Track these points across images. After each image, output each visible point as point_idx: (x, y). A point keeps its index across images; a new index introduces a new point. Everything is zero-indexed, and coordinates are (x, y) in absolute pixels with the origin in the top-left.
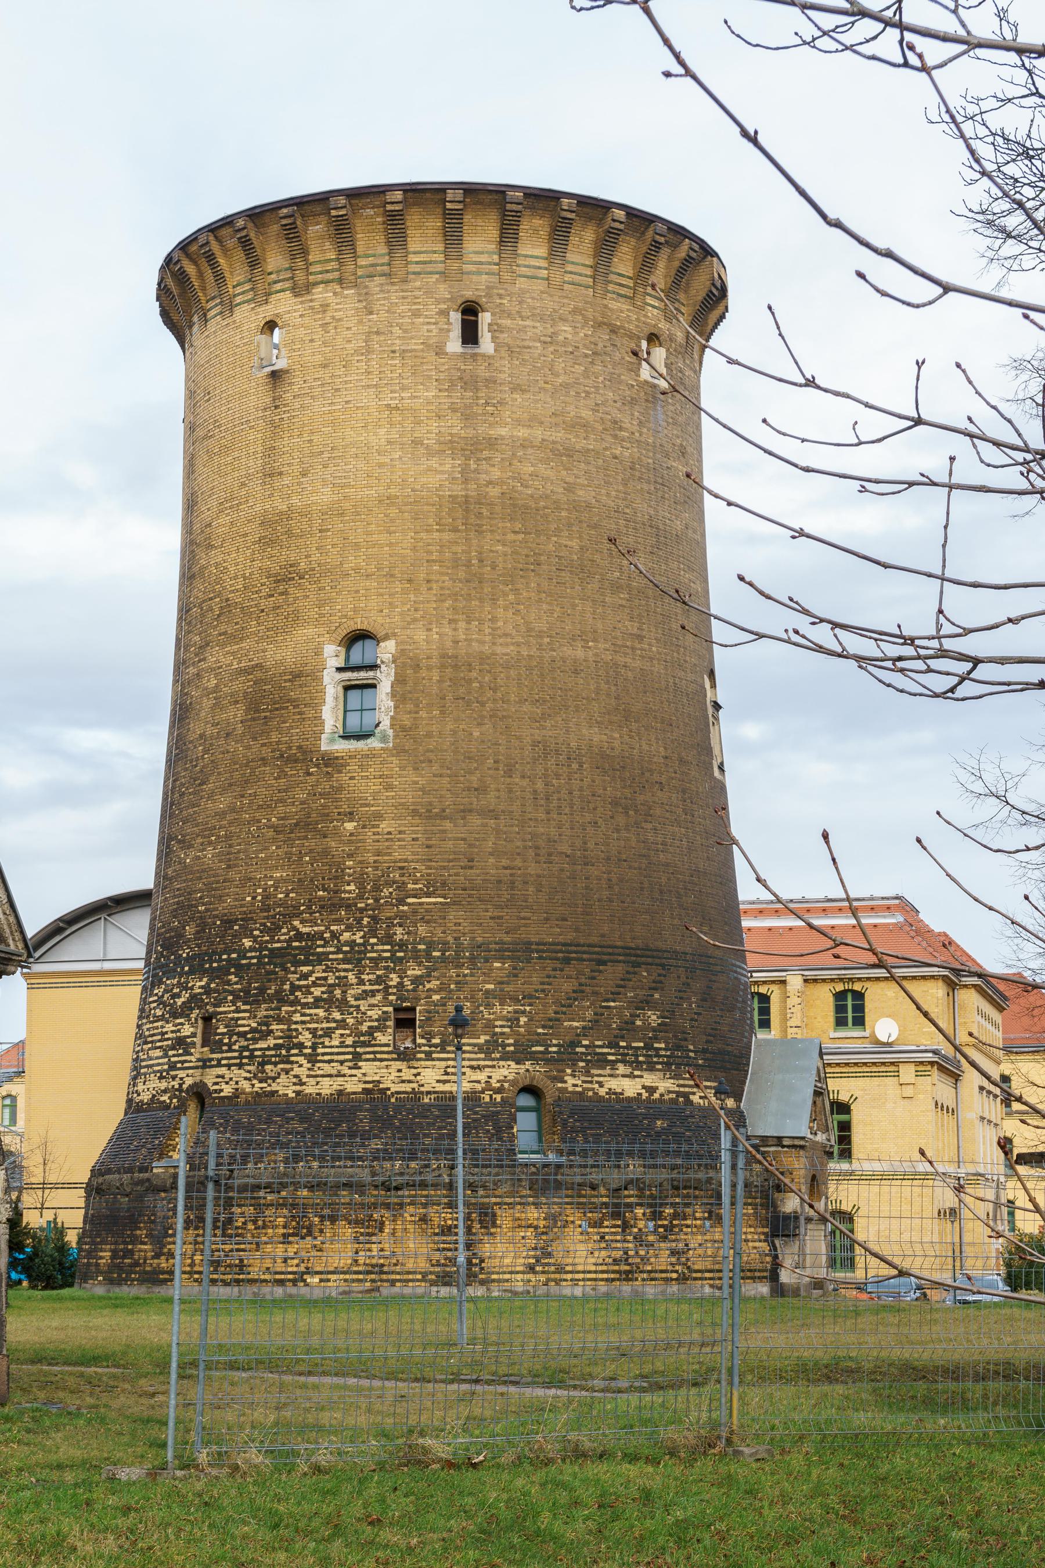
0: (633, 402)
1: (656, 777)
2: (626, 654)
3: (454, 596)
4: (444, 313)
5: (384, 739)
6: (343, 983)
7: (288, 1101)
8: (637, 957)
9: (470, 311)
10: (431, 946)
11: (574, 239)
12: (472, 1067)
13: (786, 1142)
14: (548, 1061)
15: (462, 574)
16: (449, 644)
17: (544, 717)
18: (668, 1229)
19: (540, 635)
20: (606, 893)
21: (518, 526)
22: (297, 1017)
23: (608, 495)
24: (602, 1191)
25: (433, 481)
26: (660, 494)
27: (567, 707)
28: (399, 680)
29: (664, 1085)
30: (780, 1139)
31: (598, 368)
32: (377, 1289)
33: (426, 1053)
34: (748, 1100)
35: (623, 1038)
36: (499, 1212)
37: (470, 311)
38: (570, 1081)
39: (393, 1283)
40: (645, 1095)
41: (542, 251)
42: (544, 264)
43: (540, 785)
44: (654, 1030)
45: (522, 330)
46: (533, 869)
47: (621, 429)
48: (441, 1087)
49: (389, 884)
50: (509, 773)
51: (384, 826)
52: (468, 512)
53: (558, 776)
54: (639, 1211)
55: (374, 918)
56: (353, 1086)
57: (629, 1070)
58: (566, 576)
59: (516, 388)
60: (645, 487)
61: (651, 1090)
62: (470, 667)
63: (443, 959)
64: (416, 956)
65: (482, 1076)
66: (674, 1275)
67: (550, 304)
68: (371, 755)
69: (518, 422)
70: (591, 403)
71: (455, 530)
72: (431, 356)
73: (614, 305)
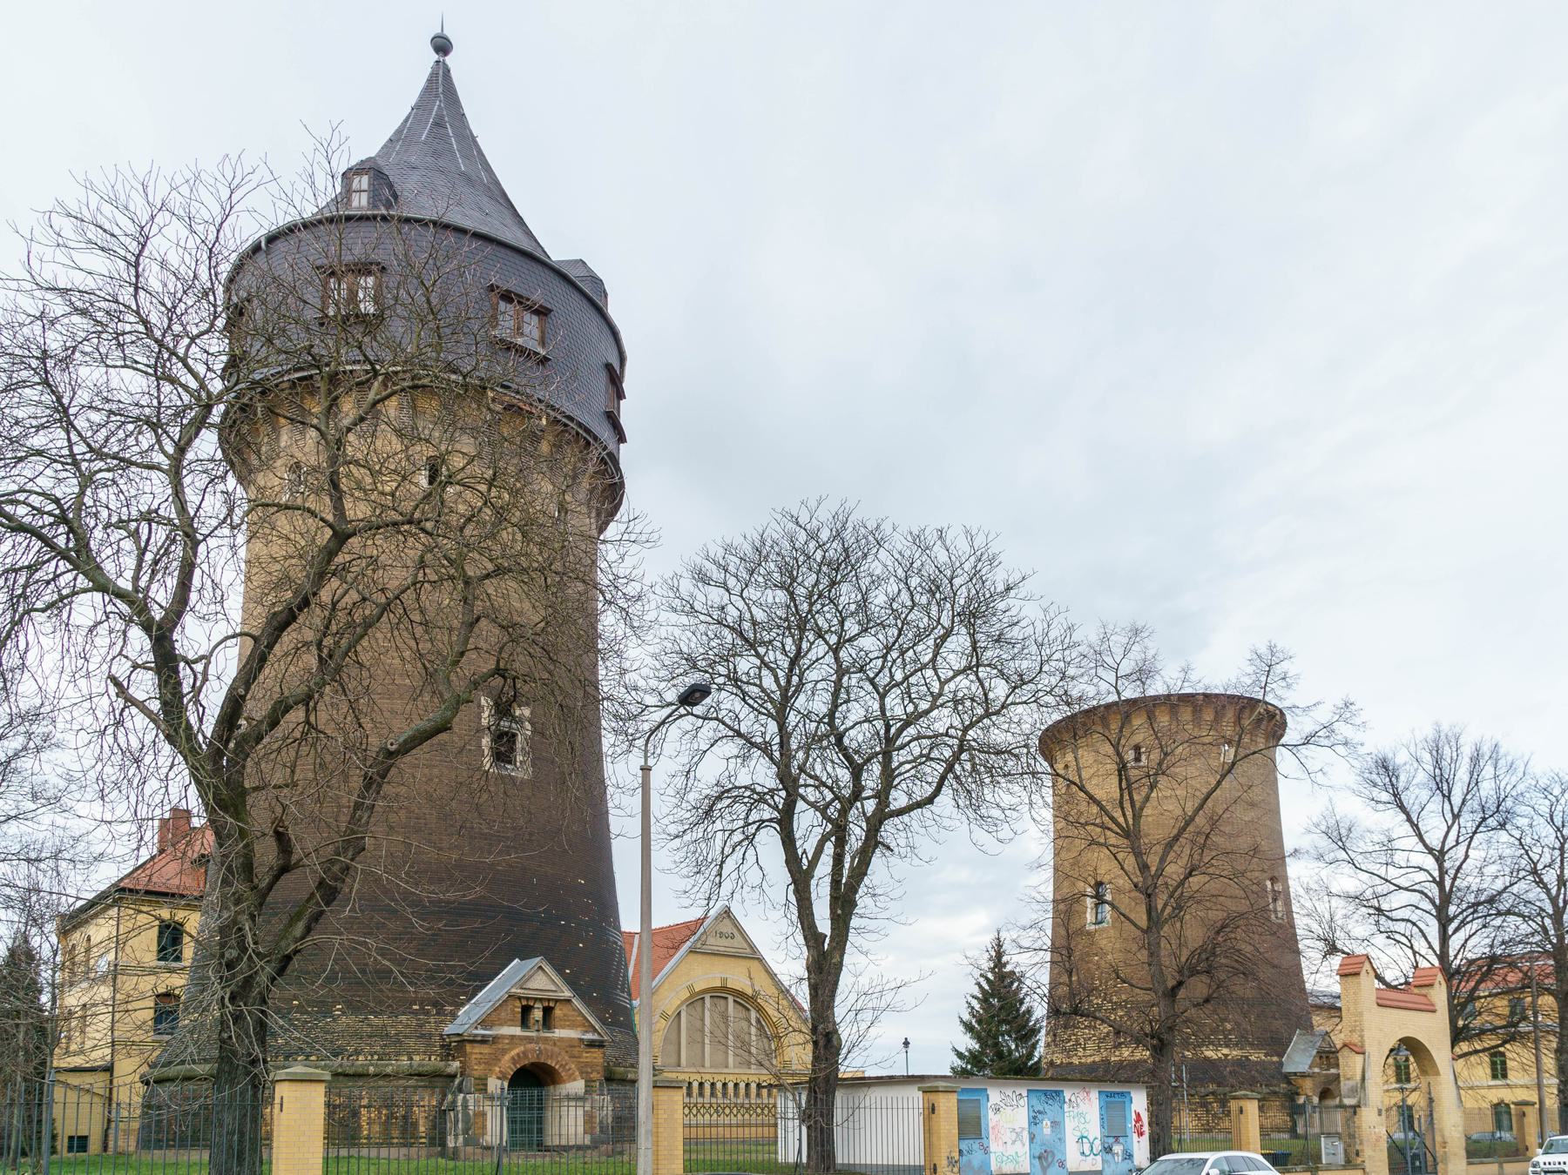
29: (1236, 1053)
68: (1104, 930)
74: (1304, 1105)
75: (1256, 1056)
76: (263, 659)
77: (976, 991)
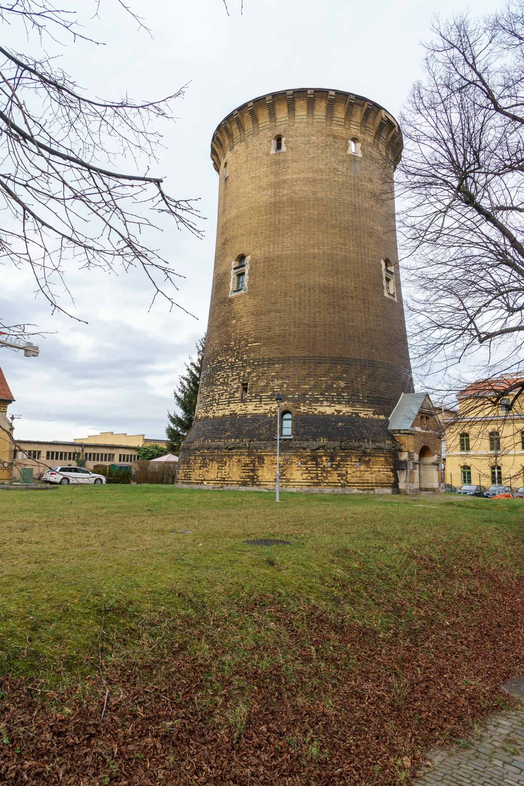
0: (344, 161)
1: (350, 294)
2: (337, 251)
3: (270, 237)
4: (270, 141)
5: (245, 290)
6: (228, 377)
7: (211, 419)
8: (334, 361)
9: (279, 139)
10: (254, 360)
11: (317, 107)
12: (265, 404)
13: (402, 432)
14: (293, 401)
15: (272, 229)
16: (267, 253)
17: (300, 275)
18: (338, 466)
19: (300, 246)
20: (323, 338)
21: (293, 208)
22: (216, 390)
23: (331, 194)
24: (308, 450)
25: (264, 199)
26: (357, 194)
27: (310, 271)
28: (251, 269)
29: (345, 410)
30: (399, 430)
31: (328, 150)
32: (222, 487)
33: (251, 400)
34: (393, 416)
35: (327, 392)
36: (266, 458)
37: (279, 139)
38: (302, 408)
39: (227, 484)
40: (336, 413)
41: (305, 113)
42: (305, 117)
43: (297, 299)
44: (342, 388)
45: (297, 141)
46: (293, 330)
47: (338, 171)
48: (254, 412)
49: (243, 340)
50: (285, 296)
51: (243, 320)
52: (275, 207)
53: (305, 296)
54: (324, 458)
55: (238, 353)
56: (227, 413)
57: (329, 404)
58: (312, 224)
59: (294, 161)
60: (349, 191)
61: (339, 412)
62: (274, 260)
63: (258, 365)
64: (249, 365)
65: (268, 407)
66: (340, 484)
67: (307, 130)
68: (241, 296)
69: (294, 173)
70: (324, 163)
71: (271, 214)
72: (265, 157)
73: (335, 128)
74: (405, 462)
75: (366, 413)
76: (460, 506)
77: (186, 374)
